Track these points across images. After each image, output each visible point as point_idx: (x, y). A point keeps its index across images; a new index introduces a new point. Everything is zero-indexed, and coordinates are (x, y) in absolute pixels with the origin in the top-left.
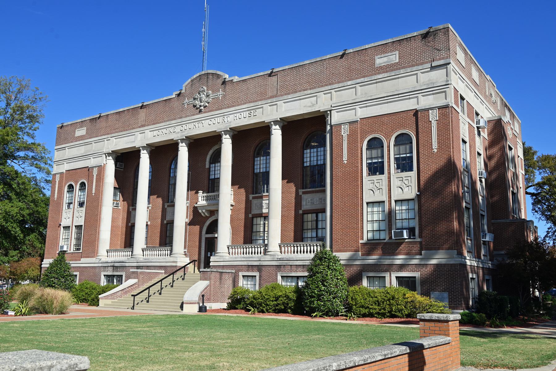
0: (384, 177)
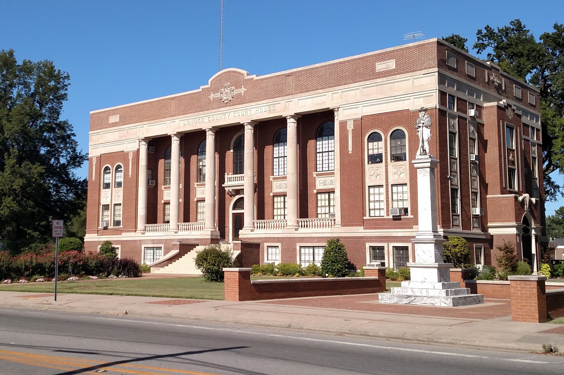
0: (383, 165)
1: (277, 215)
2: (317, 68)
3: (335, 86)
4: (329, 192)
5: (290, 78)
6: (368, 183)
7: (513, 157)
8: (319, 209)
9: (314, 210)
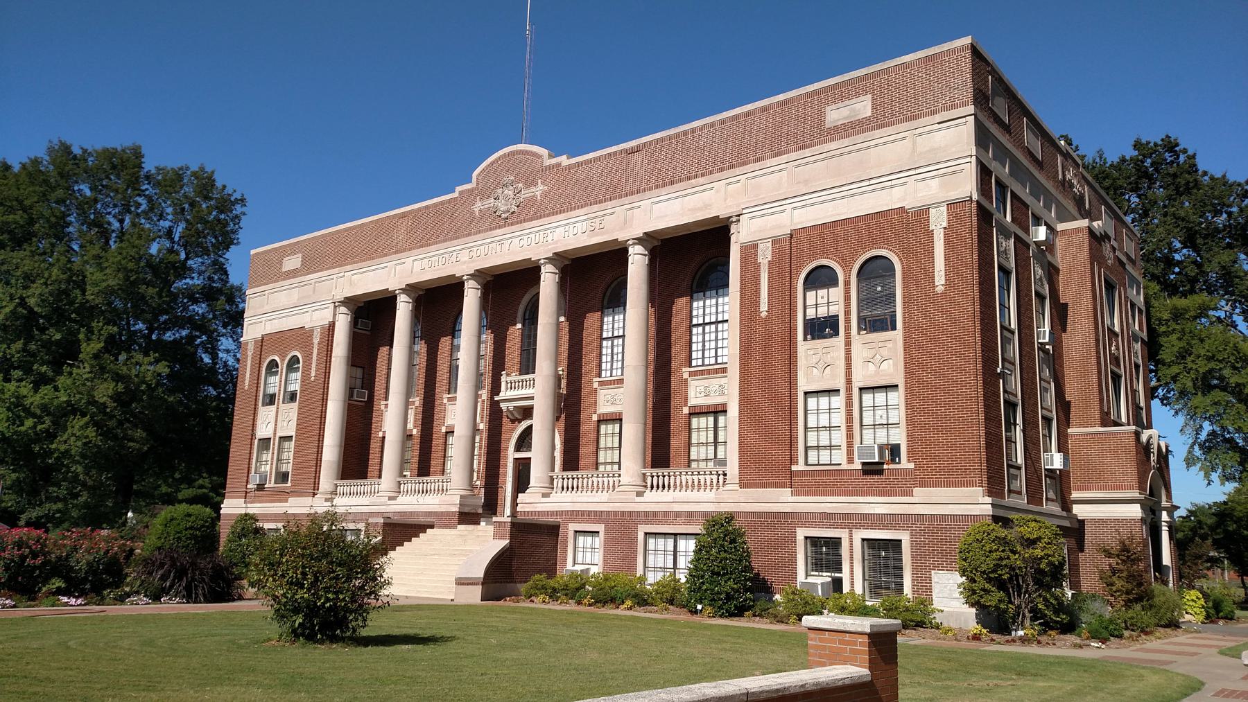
0: (839, 341)
1: (605, 463)
2: (694, 130)
3: (733, 167)
5: (637, 157)
6: (803, 385)
7: (1117, 349)
8: (694, 450)
9: (683, 451)
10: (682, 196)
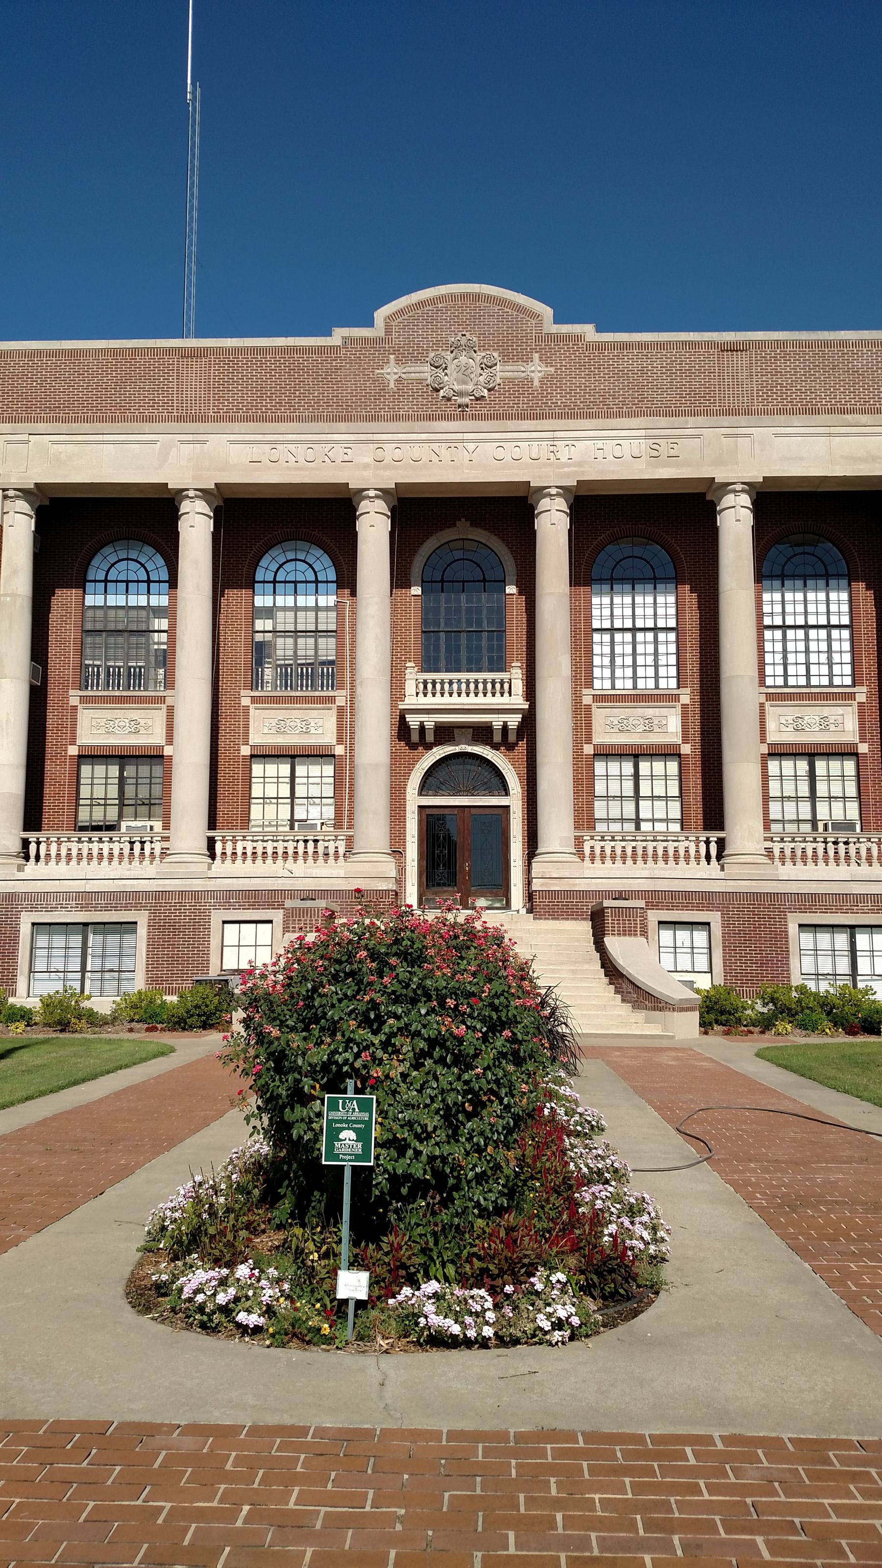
2: (843, 343)
4: (636, 756)
10: (830, 435)
